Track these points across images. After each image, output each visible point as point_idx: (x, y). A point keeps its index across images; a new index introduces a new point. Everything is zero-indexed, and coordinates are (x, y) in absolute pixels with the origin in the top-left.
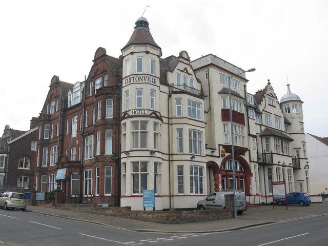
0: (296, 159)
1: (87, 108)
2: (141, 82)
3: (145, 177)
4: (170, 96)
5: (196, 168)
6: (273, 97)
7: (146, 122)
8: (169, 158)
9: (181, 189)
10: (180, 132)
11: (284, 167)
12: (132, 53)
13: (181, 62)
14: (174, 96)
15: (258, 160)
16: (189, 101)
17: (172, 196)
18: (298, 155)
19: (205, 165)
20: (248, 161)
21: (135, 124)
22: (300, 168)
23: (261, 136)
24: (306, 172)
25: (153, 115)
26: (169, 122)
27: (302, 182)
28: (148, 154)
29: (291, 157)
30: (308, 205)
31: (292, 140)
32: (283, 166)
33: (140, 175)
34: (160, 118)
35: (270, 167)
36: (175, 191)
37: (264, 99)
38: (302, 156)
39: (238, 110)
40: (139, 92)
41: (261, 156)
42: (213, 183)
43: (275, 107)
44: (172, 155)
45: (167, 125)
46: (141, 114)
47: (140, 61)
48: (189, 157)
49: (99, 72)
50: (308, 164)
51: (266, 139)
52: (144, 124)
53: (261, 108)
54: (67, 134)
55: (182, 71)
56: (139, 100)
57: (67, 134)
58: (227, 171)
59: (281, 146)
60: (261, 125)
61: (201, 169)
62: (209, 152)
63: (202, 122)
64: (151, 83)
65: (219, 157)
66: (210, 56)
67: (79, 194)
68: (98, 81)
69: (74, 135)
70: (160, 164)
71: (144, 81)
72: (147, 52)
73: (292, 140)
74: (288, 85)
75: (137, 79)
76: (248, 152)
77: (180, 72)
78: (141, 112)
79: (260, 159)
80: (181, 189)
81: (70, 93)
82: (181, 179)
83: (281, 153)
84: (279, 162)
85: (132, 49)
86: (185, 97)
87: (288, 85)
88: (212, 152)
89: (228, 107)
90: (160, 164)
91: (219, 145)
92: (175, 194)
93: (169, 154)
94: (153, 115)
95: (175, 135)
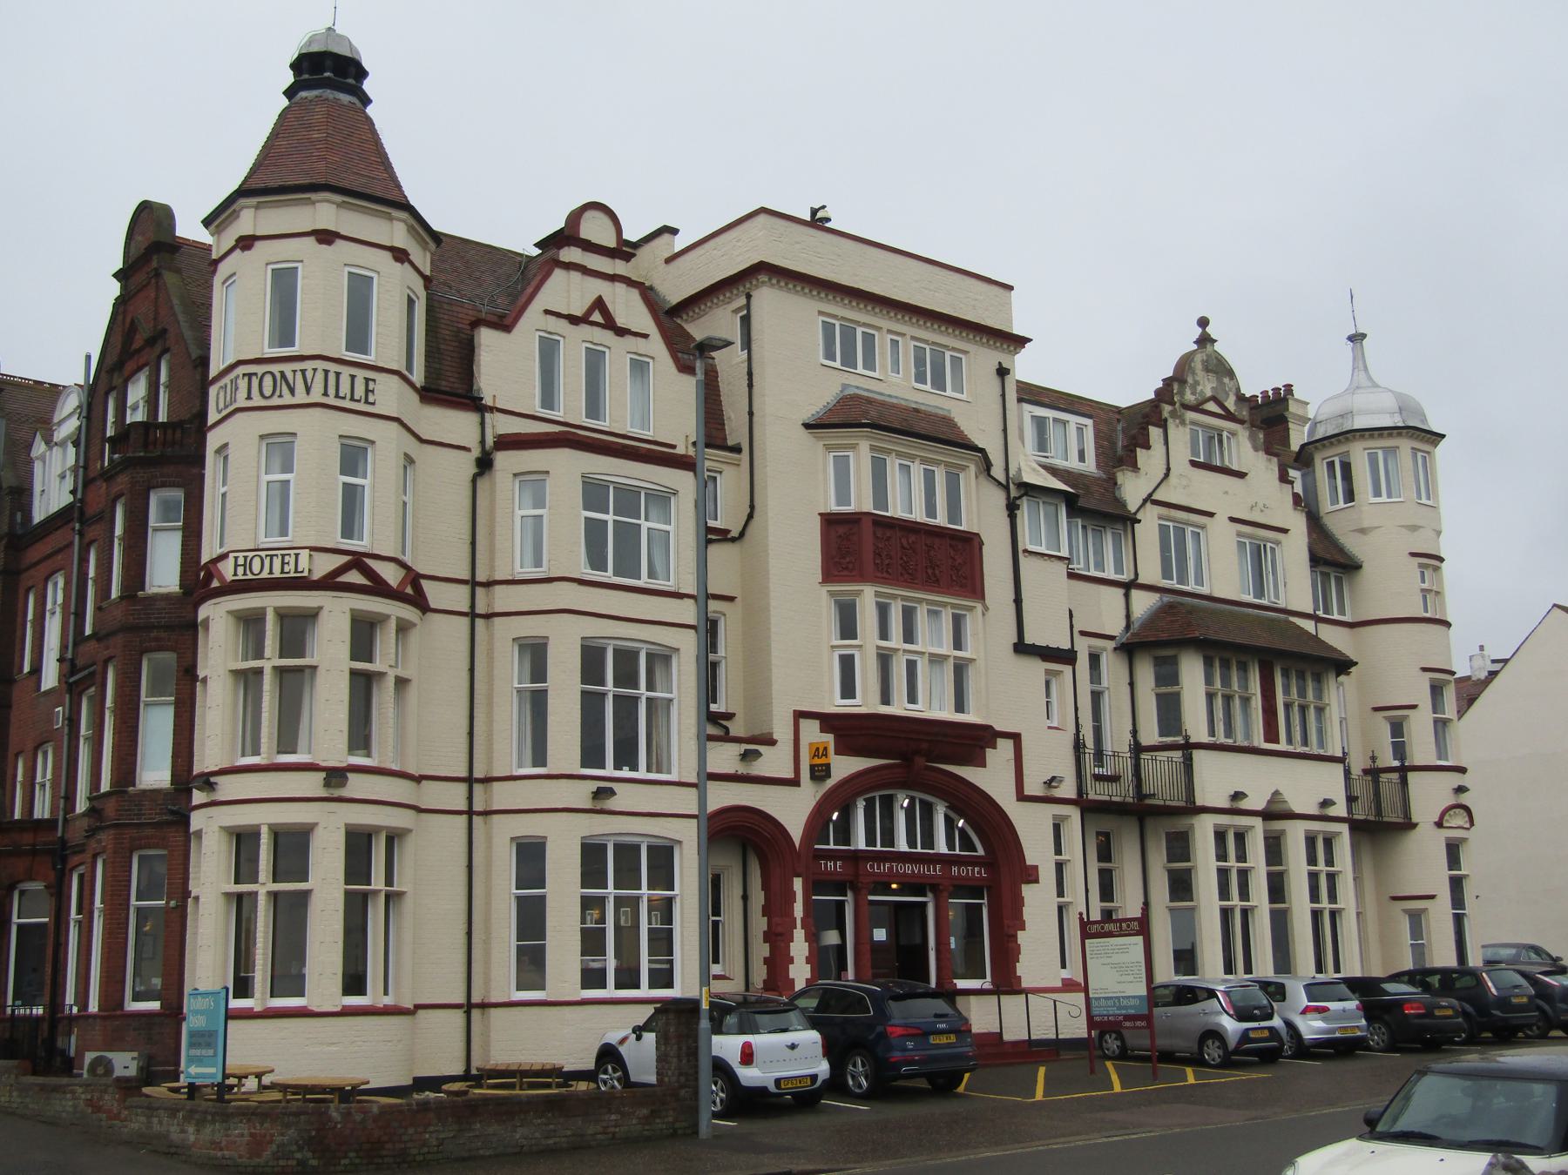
0: (1373, 773)
1: (90, 535)
2: (288, 399)
3: (291, 912)
4: (484, 464)
5: (627, 853)
7: (310, 616)
9: (532, 963)
10: (536, 654)
11: (1278, 825)
13: (569, 266)
14: (506, 461)
16: (594, 494)
17: (484, 1006)
18: (1399, 750)
19: (687, 837)
21: (251, 622)
22: (1409, 825)
23: (1130, 649)
24: (1453, 851)
25: (354, 577)
26: (473, 606)
28: (311, 784)
29: (1341, 760)
30: (943, 1082)
31: (1343, 665)
33: (262, 901)
34: (413, 592)
35: (1180, 824)
36: (501, 978)
37: (1155, 433)
38: (1422, 749)
39: (931, 510)
40: (353, 456)
41: (1362, 788)
42: (760, 924)
43: (1241, 475)
44: (488, 780)
45: (464, 622)
46: (277, 574)
47: (284, 283)
48: (580, 794)
49: (138, 342)
50: (1465, 799)
51: (1159, 662)
52: (296, 628)
53: (1133, 489)
54: (27, 669)
55: (574, 320)
56: (351, 496)
57: (27, 669)
58: (857, 856)
59: (1257, 703)
60: (1128, 587)
61: (663, 857)
62: (724, 758)
65: (794, 782)
66: (762, 218)
67: (47, 999)
68: (137, 391)
69: (50, 678)
70: (394, 838)
71: (301, 397)
72: (326, 237)
73: (1343, 665)
74: (1357, 338)
75: (268, 381)
76: (1005, 746)
77: (563, 325)
78: (277, 563)
80: (532, 963)
81: (39, 447)
82: (531, 918)
83: (1259, 741)
84: (1238, 796)
85: (248, 221)
86: (567, 467)
87: (1357, 338)
88: (746, 756)
89: (861, 501)
90: (394, 838)
91: (799, 715)
92: (495, 998)
93: (470, 780)
94: (354, 577)
95: (508, 674)
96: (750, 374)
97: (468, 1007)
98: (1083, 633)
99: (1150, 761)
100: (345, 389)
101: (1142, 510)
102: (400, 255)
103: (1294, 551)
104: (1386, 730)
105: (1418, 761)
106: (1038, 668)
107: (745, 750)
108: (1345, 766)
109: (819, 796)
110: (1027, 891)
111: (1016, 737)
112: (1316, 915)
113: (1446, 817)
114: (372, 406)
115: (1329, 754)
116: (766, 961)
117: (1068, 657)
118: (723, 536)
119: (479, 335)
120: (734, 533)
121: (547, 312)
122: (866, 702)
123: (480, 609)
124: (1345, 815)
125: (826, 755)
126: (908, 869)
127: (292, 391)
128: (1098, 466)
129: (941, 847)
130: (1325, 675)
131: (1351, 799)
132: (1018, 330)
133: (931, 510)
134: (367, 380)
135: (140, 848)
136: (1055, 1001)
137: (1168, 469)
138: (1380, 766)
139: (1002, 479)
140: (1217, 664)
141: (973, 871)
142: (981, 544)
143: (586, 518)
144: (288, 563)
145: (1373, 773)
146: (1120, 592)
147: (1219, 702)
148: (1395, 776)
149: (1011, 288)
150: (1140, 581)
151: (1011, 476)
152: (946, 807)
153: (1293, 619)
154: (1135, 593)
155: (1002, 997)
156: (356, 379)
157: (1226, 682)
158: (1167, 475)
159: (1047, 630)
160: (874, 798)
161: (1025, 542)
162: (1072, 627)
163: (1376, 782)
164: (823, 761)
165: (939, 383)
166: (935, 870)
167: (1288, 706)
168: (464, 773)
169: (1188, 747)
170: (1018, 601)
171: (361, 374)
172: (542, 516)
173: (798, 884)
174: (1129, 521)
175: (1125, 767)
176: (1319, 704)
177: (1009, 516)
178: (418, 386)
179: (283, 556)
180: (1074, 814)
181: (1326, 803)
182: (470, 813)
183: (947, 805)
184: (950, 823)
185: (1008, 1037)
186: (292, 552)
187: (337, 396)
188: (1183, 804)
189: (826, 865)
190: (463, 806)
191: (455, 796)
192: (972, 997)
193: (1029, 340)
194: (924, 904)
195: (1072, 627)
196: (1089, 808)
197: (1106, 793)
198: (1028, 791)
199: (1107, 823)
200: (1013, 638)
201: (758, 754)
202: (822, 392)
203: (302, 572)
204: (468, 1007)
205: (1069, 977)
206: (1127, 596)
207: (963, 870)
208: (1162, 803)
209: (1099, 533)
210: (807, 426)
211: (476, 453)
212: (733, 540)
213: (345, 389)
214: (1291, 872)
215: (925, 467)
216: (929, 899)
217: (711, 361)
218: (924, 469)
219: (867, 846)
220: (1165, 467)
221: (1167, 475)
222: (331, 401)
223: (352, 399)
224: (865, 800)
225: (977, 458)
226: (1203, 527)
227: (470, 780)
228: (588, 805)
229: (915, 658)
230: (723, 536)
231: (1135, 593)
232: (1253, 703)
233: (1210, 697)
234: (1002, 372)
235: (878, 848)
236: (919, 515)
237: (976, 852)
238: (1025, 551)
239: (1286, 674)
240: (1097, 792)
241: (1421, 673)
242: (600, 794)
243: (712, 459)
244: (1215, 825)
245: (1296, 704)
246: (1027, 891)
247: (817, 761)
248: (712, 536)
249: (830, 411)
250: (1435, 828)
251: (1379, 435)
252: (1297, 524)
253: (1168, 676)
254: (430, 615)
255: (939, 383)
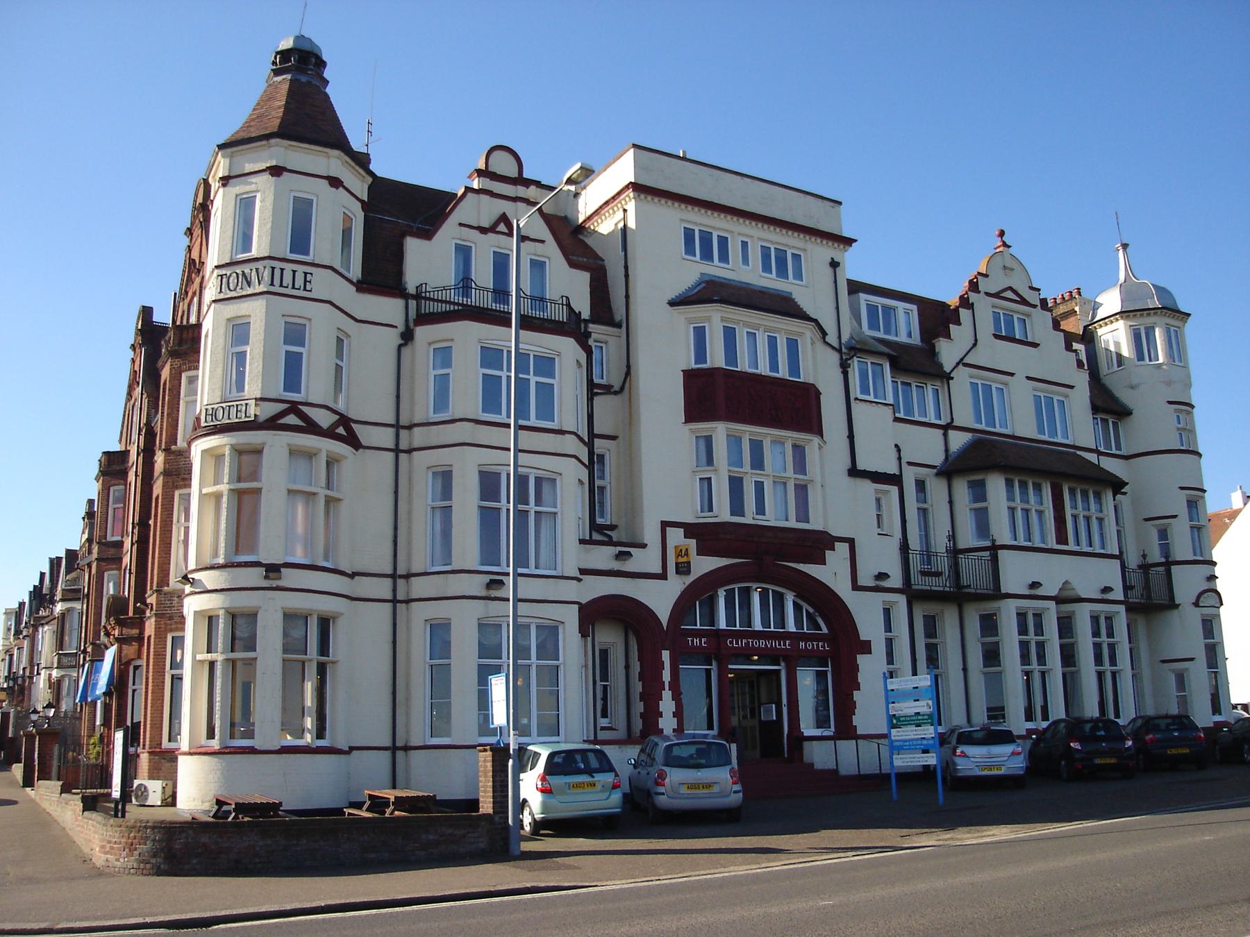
6: (1024, 302)
8: (394, 590)
10: (445, 478)
12: (276, 171)
15: (1126, 595)
17: (406, 748)
18: (1165, 549)
19: (570, 618)
20: (842, 587)
22: (1172, 605)
25: (292, 419)
26: (397, 444)
27: (1186, 664)
31: (1117, 486)
32: (1059, 600)
35: (990, 607)
38: (1182, 548)
39: (774, 366)
41: (1136, 579)
42: (638, 687)
44: (408, 576)
45: (391, 455)
48: (475, 585)
55: (483, 230)
58: (789, 635)
60: (946, 428)
61: (550, 633)
62: (602, 557)
63: (561, 432)
64: (290, 291)
65: (663, 576)
75: (233, 280)
79: (1132, 588)
84: (1035, 585)
89: (716, 358)
91: (665, 525)
92: (415, 741)
93: (394, 576)
94: (292, 419)
95: (423, 492)
96: (626, 267)
97: (394, 749)
98: (910, 463)
99: (963, 559)
100: (288, 279)
101: (956, 370)
102: (335, 182)
103: (1081, 396)
104: (1154, 535)
105: (1179, 557)
106: (868, 487)
107: (619, 551)
108: (1121, 562)
109: (683, 587)
110: (862, 660)
111: (851, 542)
112: (1100, 675)
113: (1202, 599)
114: (309, 293)
115: (1109, 552)
116: (642, 715)
117: (895, 480)
118: (607, 389)
119: (406, 242)
120: (616, 388)
121: (461, 225)
122: (722, 513)
123: (403, 446)
124: (1122, 599)
125: (687, 554)
126: (762, 643)
127: (249, 284)
128: (922, 340)
129: (791, 627)
130: (1104, 492)
131: (1127, 588)
132: (846, 233)
133: (774, 366)
134: (306, 274)
135: (171, 630)
136: (878, 744)
137: (976, 340)
138: (1149, 562)
139: (836, 344)
140: (1016, 484)
141: (818, 645)
142: (818, 393)
143: (483, 374)
144: (240, 411)
145: (1145, 567)
146: (940, 432)
147: (1019, 514)
148: (1161, 569)
149: (840, 203)
150: (954, 424)
151: (843, 341)
152: (794, 596)
153: (1078, 453)
154: (951, 433)
155: (837, 742)
156: (284, 271)
157: (1025, 500)
158: (975, 345)
159: (876, 458)
160: (734, 588)
161: (856, 391)
162: (900, 459)
163: (1146, 574)
164: (685, 559)
165: (782, 272)
166: (785, 645)
167: (1075, 517)
168: (389, 571)
169: (994, 549)
170: (851, 437)
171: (301, 269)
172: (448, 374)
173: (666, 655)
174: (947, 377)
175: (943, 564)
176: (1100, 515)
177: (842, 372)
178: (355, 281)
179: (237, 405)
180: (901, 600)
181: (1107, 590)
182: (394, 601)
183: (795, 594)
184: (797, 607)
185: (843, 771)
186: (243, 402)
187: (281, 285)
188: (991, 592)
189: (692, 641)
190: (389, 596)
191: (383, 588)
192: (814, 742)
193: (855, 241)
194: (779, 671)
195: (900, 459)
196: (914, 596)
197: (941, 585)
198: (861, 582)
199: (932, 608)
200: (847, 463)
201: (629, 554)
202: (690, 273)
203: (250, 417)
204: (394, 749)
205: (1035, 727)
206: (945, 435)
207: (809, 645)
208: (974, 591)
209: (922, 389)
210: (672, 303)
211: (401, 328)
212: (616, 393)
213: (288, 279)
214: (1079, 643)
215: (769, 334)
216: (781, 667)
217: (601, 262)
218: (768, 336)
219: (727, 626)
220: (973, 339)
221: (975, 345)
222: (277, 289)
223: (293, 287)
224: (725, 591)
225: (811, 327)
226: (1006, 384)
227: (394, 576)
228: (483, 593)
229: (762, 480)
230: (607, 389)
231: (951, 433)
232: (1047, 513)
233: (1012, 510)
234: (834, 265)
235: (772, 629)
236: (763, 369)
237: (822, 630)
238: (856, 399)
239: (1072, 492)
240: (919, 583)
241: (1179, 490)
242: (492, 584)
243: (598, 331)
244: (1017, 608)
245: (1082, 516)
246: (862, 660)
247: (681, 560)
248: (593, 389)
249: (247, 125)
250: (1193, 607)
251: (1154, 314)
252: (1081, 380)
253: (979, 492)
254: (361, 450)
255: (782, 272)
